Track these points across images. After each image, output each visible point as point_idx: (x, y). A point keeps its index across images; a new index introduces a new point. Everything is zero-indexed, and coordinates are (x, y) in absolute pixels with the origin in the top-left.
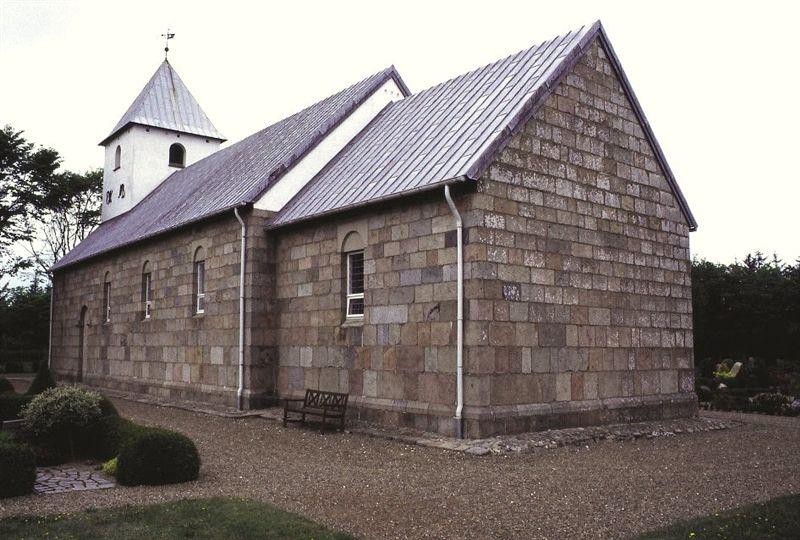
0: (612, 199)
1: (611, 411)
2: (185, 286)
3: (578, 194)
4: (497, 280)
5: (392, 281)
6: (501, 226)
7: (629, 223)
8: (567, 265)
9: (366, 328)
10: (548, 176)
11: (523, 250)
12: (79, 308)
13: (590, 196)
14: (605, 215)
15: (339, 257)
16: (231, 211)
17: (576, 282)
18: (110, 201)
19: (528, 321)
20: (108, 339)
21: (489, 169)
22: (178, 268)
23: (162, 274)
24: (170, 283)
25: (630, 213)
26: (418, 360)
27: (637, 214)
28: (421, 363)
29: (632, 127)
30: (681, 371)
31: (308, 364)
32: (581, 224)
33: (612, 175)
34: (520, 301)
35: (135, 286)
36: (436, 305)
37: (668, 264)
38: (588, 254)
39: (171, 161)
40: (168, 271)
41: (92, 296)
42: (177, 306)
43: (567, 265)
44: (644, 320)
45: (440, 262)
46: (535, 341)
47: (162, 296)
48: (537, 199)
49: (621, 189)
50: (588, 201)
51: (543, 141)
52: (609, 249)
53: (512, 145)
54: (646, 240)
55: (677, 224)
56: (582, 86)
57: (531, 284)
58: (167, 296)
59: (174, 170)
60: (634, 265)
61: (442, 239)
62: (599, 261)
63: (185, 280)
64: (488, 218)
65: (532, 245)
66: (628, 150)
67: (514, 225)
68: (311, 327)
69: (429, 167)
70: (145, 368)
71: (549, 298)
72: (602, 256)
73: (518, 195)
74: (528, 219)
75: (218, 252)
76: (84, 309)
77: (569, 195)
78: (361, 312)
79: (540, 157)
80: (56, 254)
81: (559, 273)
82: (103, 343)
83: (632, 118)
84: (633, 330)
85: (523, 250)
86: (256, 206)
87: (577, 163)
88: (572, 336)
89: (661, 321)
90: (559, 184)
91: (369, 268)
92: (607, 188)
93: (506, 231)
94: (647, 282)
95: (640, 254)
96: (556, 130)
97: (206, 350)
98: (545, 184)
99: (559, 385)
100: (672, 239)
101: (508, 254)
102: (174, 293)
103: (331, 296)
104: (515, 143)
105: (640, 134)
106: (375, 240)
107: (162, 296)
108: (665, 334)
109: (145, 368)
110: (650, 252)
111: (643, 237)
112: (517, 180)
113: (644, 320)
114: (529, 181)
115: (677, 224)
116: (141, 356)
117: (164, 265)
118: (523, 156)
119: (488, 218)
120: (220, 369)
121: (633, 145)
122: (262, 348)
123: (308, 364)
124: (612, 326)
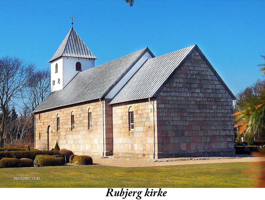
0: (201, 95)
1: (200, 153)
2: (86, 120)
3: (188, 95)
4: (162, 120)
5: (140, 120)
6: (164, 107)
7: (208, 101)
8: (185, 115)
9: (134, 132)
10: (178, 92)
11: (170, 112)
12: (47, 126)
13: (193, 95)
14: (198, 100)
15: (128, 113)
16: (99, 99)
17: (188, 119)
18: (54, 84)
19: (172, 130)
20: (59, 137)
21: (160, 93)
22: (83, 114)
23: (78, 116)
24: (81, 119)
25: (208, 98)
26: (146, 140)
27: (210, 98)
28: (146, 141)
29: (210, 73)
30: (228, 142)
31: (121, 143)
32: (190, 103)
33: (201, 88)
34: (169, 125)
35: (69, 119)
36: (149, 127)
37: (223, 111)
38: (192, 111)
39: (76, 69)
40: (80, 115)
41: (52, 122)
42: (83, 126)
43: (185, 115)
44: (213, 128)
45: (149, 116)
46: (174, 135)
47: (78, 123)
48: (175, 99)
49: (205, 91)
50: (192, 97)
51: (177, 83)
52: (199, 109)
53: (164, 90)
54: (214, 105)
55: (227, 99)
56: (190, 65)
57: (173, 120)
58: (80, 123)
59: (77, 72)
60: (210, 113)
61: (150, 110)
62: (196, 113)
63: (86, 118)
64: (160, 105)
65: (173, 110)
66: (208, 80)
67: (167, 106)
68: (122, 132)
69: (166, 69)
70: (73, 146)
71: (178, 123)
72: (197, 111)
73: (169, 98)
74: (172, 104)
75: (96, 110)
76: (49, 126)
77: (186, 96)
78: (133, 128)
79: (176, 87)
80: (33, 104)
81: (182, 117)
82: (57, 139)
83: (209, 70)
84: (209, 131)
85: (170, 112)
86: (105, 98)
87: (188, 87)
88: (187, 133)
89: (219, 127)
90: (182, 94)
91: (135, 116)
92: (199, 92)
93: (165, 108)
94: (214, 117)
95: (212, 109)
96: (181, 79)
97: (93, 140)
98: (177, 94)
99: (182, 146)
100: (225, 104)
101: (165, 114)
102: (82, 122)
103: (126, 124)
104: (167, 85)
105: (213, 74)
106: (136, 109)
107: (78, 123)
108: (222, 131)
109: (73, 146)
110: (216, 108)
111: (213, 104)
112: (168, 95)
113: (213, 128)
114: (172, 94)
115: (227, 99)
116: (72, 142)
117: (78, 113)
118: (170, 88)
119: (160, 105)
120: (97, 145)
121: (209, 78)
122: (109, 139)
123: (121, 143)
124: (201, 130)
